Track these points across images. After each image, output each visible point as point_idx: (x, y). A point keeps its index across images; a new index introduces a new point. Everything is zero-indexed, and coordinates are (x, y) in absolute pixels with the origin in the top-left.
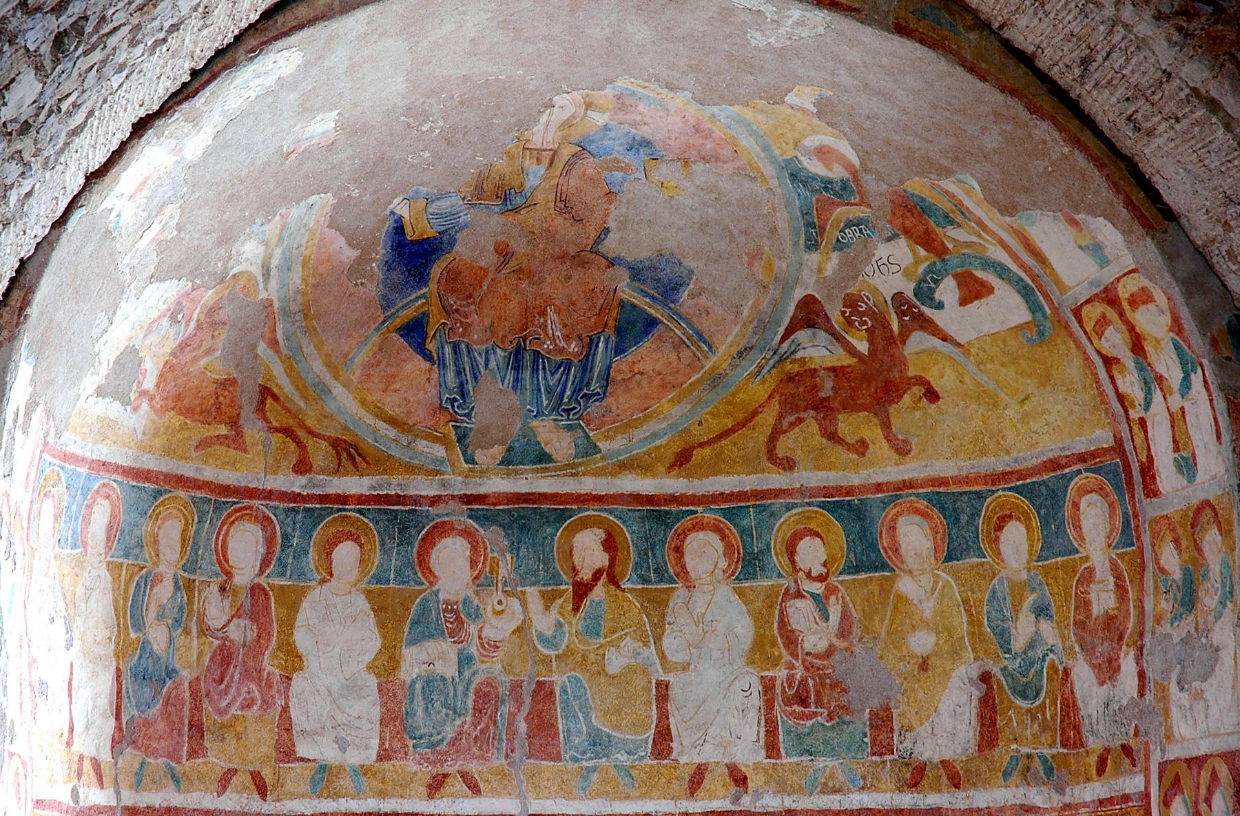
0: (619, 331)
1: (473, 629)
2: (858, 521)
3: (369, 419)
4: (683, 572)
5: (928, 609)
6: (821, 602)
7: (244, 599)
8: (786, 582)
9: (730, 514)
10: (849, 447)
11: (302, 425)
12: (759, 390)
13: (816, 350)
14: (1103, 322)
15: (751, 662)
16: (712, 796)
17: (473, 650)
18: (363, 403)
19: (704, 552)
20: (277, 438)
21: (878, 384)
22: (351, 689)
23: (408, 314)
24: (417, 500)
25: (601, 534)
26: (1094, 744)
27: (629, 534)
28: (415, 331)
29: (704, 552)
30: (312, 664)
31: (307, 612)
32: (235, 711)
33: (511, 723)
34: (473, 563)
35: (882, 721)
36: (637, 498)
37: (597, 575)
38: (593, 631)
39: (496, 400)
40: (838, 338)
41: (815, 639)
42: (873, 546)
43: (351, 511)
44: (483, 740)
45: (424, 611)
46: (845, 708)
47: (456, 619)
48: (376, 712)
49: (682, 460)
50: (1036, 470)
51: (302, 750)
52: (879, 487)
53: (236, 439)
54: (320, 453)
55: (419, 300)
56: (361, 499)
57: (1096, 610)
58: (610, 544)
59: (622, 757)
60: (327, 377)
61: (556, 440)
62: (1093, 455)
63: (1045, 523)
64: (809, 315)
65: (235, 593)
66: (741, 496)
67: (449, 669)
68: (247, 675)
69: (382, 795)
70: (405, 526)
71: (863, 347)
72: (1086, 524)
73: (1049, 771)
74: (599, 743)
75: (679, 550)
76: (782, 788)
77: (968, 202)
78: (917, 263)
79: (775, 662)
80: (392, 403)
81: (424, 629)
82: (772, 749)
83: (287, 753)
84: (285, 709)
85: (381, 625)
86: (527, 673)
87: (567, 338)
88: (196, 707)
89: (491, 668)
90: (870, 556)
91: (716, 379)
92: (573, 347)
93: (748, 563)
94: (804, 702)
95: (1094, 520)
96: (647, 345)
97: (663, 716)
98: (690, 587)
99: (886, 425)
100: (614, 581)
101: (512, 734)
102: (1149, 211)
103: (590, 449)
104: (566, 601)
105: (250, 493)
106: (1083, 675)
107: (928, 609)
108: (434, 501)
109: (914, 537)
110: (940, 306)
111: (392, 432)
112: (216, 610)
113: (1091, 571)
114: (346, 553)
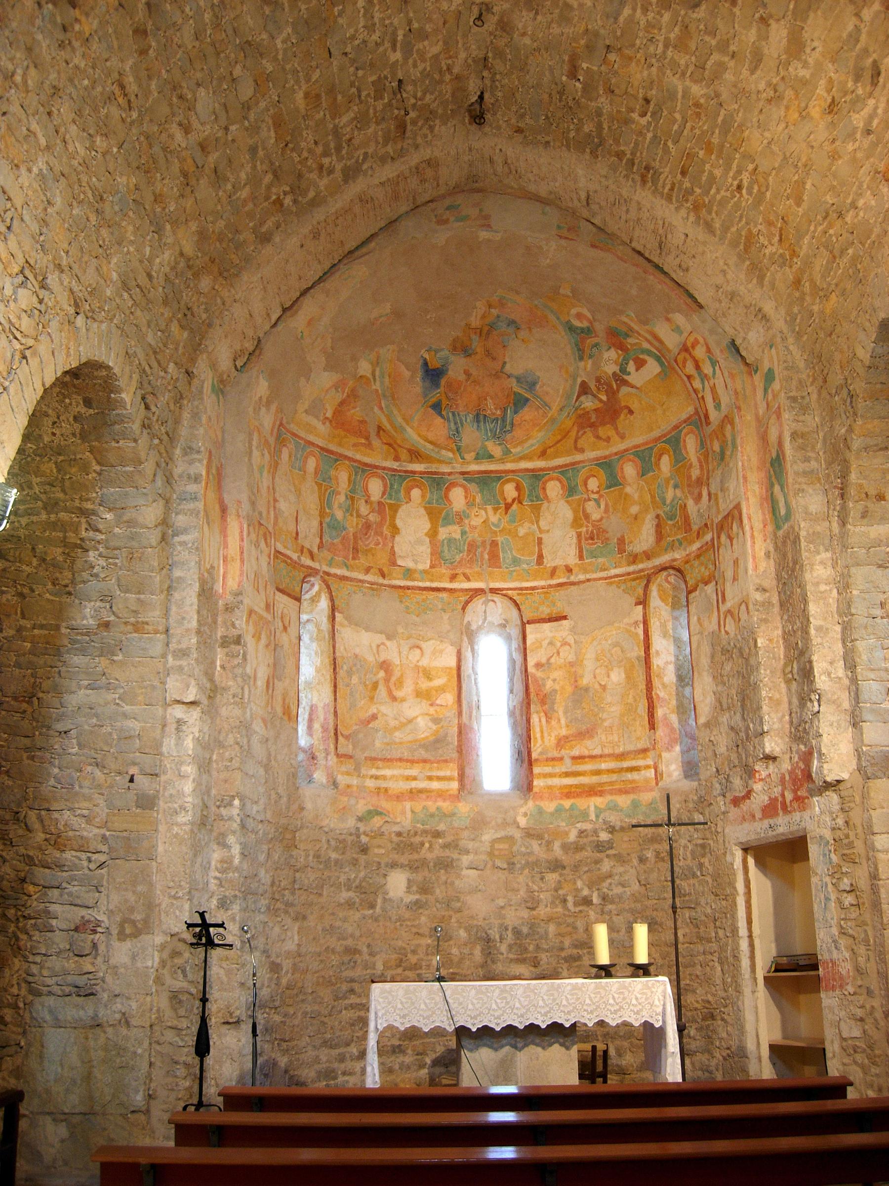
0: (515, 404)
1: (466, 521)
2: (608, 467)
3: (422, 442)
4: (546, 497)
5: (636, 496)
6: (597, 502)
7: (376, 506)
8: (585, 496)
9: (562, 473)
10: (604, 440)
11: (395, 442)
12: (569, 423)
13: (588, 403)
14: (685, 361)
15: (572, 527)
16: (559, 577)
17: (467, 529)
18: (419, 435)
19: (554, 488)
20: (385, 447)
21: (611, 412)
22: (419, 542)
23: (434, 400)
24: (443, 474)
25: (514, 485)
26: (695, 528)
27: (525, 484)
28: (437, 407)
29: (554, 488)
30: (403, 532)
31: (401, 513)
32: (372, 546)
33: (482, 556)
34: (466, 497)
35: (621, 541)
36: (527, 470)
37: (514, 500)
38: (512, 521)
39: (471, 435)
40: (595, 396)
41: (595, 516)
42: (615, 477)
43: (417, 477)
44: (471, 561)
45: (447, 515)
46: (607, 539)
47: (460, 518)
48: (429, 551)
49: (543, 454)
50: (670, 432)
51: (399, 562)
52: (616, 454)
53: (369, 445)
54: (404, 455)
55: (436, 395)
56: (421, 473)
57: (694, 478)
58: (518, 488)
59: (525, 566)
60: (404, 424)
61: (496, 450)
62: (688, 418)
63: (675, 451)
64: (584, 389)
65: (372, 503)
66: (566, 465)
67: (457, 536)
68: (376, 533)
69: (432, 581)
70: (438, 483)
71: (604, 398)
72: (688, 446)
73: (680, 544)
74: (516, 561)
75: (544, 489)
76: (585, 571)
77: (632, 325)
78: (619, 356)
79: (581, 526)
80: (431, 436)
81: (447, 521)
82: (581, 557)
83: (394, 563)
84: (393, 547)
85: (431, 519)
86: (488, 538)
87: (496, 409)
88: (356, 542)
89: (474, 536)
90: (614, 481)
91: (553, 420)
92: (499, 412)
93: (570, 491)
94: (592, 539)
95: (691, 445)
96: (526, 409)
97: (540, 550)
98: (549, 502)
99: (616, 429)
100: (520, 502)
101: (482, 559)
102: (694, 306)
103: (507, 452)
104: (502, 510)
105: (377, 467)
106: (690, 503)
107: (636, 496)
108: (450, 474)
109: (630, 470)
110: (629, 374)
111: (431, 447)
112: (364, 509)
113: (691, 465)
114: (416, 493)
